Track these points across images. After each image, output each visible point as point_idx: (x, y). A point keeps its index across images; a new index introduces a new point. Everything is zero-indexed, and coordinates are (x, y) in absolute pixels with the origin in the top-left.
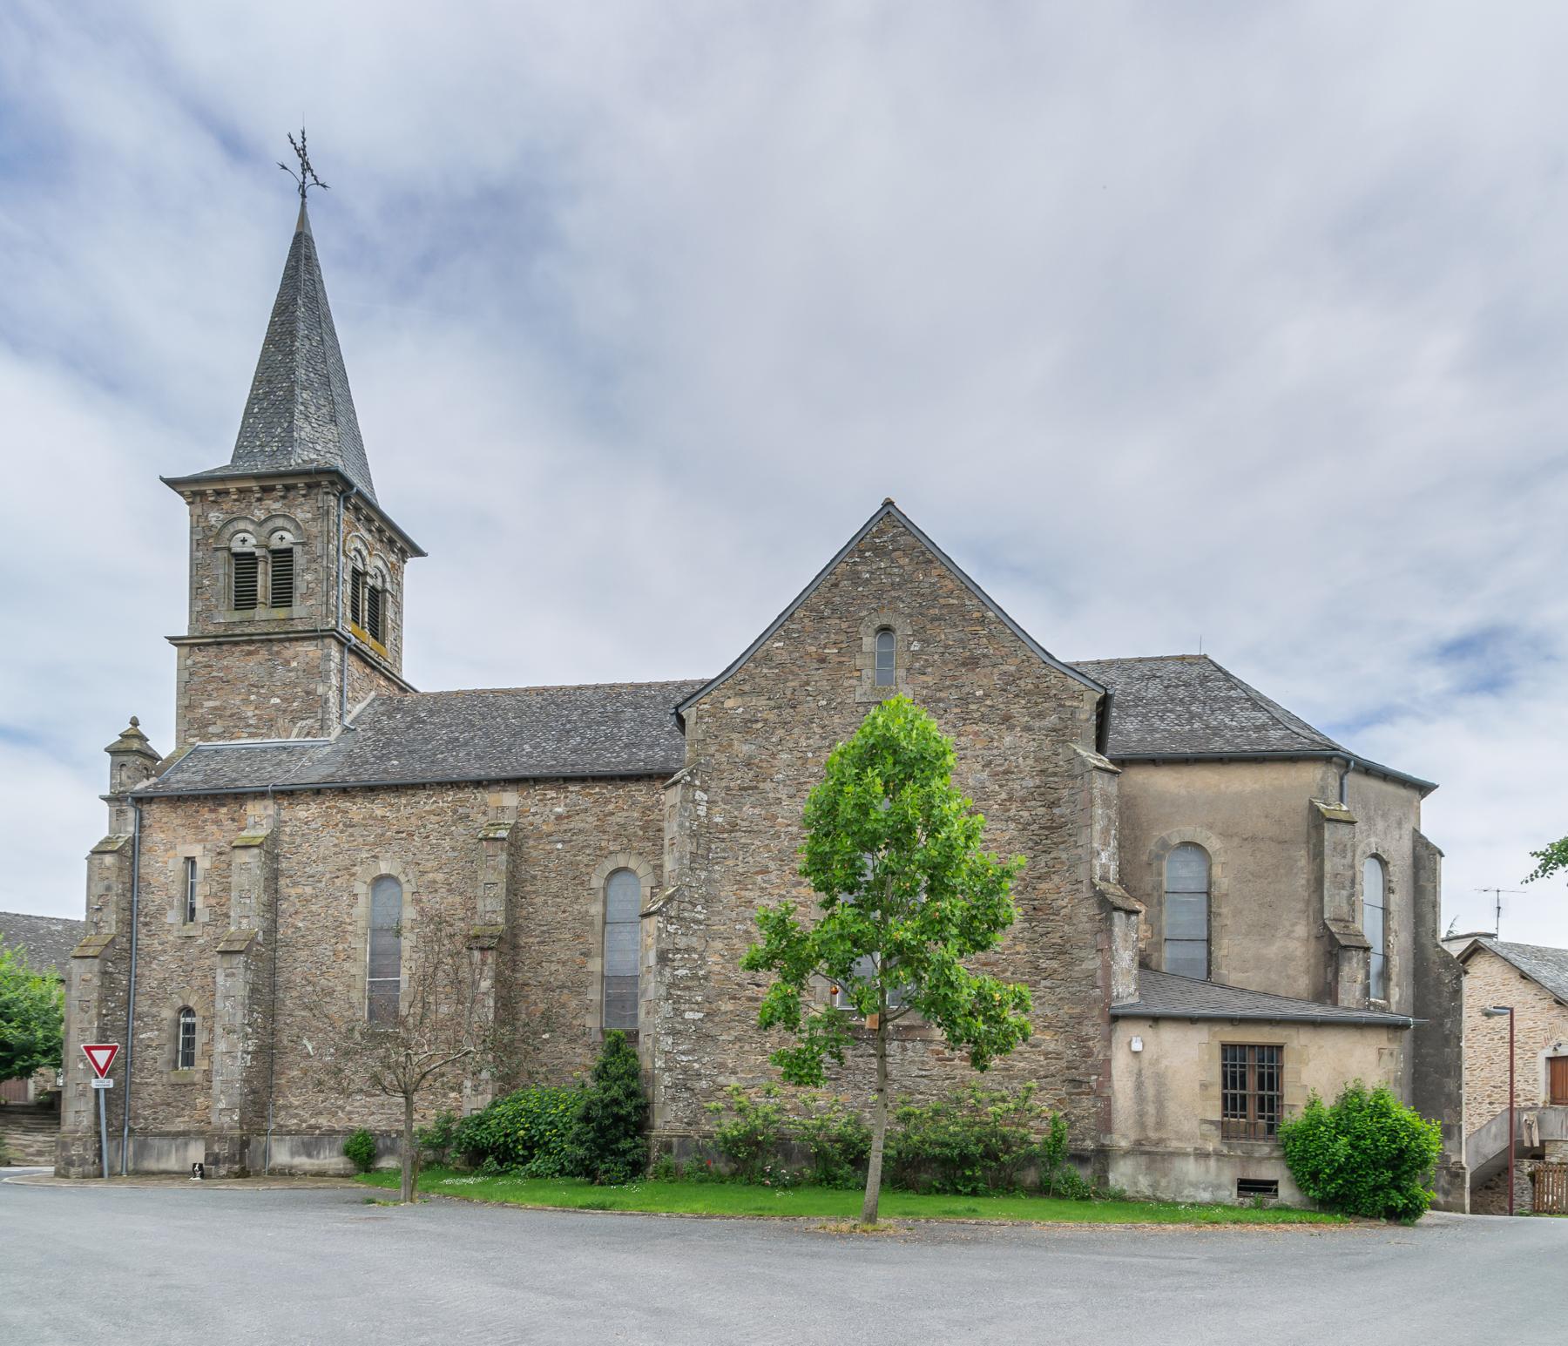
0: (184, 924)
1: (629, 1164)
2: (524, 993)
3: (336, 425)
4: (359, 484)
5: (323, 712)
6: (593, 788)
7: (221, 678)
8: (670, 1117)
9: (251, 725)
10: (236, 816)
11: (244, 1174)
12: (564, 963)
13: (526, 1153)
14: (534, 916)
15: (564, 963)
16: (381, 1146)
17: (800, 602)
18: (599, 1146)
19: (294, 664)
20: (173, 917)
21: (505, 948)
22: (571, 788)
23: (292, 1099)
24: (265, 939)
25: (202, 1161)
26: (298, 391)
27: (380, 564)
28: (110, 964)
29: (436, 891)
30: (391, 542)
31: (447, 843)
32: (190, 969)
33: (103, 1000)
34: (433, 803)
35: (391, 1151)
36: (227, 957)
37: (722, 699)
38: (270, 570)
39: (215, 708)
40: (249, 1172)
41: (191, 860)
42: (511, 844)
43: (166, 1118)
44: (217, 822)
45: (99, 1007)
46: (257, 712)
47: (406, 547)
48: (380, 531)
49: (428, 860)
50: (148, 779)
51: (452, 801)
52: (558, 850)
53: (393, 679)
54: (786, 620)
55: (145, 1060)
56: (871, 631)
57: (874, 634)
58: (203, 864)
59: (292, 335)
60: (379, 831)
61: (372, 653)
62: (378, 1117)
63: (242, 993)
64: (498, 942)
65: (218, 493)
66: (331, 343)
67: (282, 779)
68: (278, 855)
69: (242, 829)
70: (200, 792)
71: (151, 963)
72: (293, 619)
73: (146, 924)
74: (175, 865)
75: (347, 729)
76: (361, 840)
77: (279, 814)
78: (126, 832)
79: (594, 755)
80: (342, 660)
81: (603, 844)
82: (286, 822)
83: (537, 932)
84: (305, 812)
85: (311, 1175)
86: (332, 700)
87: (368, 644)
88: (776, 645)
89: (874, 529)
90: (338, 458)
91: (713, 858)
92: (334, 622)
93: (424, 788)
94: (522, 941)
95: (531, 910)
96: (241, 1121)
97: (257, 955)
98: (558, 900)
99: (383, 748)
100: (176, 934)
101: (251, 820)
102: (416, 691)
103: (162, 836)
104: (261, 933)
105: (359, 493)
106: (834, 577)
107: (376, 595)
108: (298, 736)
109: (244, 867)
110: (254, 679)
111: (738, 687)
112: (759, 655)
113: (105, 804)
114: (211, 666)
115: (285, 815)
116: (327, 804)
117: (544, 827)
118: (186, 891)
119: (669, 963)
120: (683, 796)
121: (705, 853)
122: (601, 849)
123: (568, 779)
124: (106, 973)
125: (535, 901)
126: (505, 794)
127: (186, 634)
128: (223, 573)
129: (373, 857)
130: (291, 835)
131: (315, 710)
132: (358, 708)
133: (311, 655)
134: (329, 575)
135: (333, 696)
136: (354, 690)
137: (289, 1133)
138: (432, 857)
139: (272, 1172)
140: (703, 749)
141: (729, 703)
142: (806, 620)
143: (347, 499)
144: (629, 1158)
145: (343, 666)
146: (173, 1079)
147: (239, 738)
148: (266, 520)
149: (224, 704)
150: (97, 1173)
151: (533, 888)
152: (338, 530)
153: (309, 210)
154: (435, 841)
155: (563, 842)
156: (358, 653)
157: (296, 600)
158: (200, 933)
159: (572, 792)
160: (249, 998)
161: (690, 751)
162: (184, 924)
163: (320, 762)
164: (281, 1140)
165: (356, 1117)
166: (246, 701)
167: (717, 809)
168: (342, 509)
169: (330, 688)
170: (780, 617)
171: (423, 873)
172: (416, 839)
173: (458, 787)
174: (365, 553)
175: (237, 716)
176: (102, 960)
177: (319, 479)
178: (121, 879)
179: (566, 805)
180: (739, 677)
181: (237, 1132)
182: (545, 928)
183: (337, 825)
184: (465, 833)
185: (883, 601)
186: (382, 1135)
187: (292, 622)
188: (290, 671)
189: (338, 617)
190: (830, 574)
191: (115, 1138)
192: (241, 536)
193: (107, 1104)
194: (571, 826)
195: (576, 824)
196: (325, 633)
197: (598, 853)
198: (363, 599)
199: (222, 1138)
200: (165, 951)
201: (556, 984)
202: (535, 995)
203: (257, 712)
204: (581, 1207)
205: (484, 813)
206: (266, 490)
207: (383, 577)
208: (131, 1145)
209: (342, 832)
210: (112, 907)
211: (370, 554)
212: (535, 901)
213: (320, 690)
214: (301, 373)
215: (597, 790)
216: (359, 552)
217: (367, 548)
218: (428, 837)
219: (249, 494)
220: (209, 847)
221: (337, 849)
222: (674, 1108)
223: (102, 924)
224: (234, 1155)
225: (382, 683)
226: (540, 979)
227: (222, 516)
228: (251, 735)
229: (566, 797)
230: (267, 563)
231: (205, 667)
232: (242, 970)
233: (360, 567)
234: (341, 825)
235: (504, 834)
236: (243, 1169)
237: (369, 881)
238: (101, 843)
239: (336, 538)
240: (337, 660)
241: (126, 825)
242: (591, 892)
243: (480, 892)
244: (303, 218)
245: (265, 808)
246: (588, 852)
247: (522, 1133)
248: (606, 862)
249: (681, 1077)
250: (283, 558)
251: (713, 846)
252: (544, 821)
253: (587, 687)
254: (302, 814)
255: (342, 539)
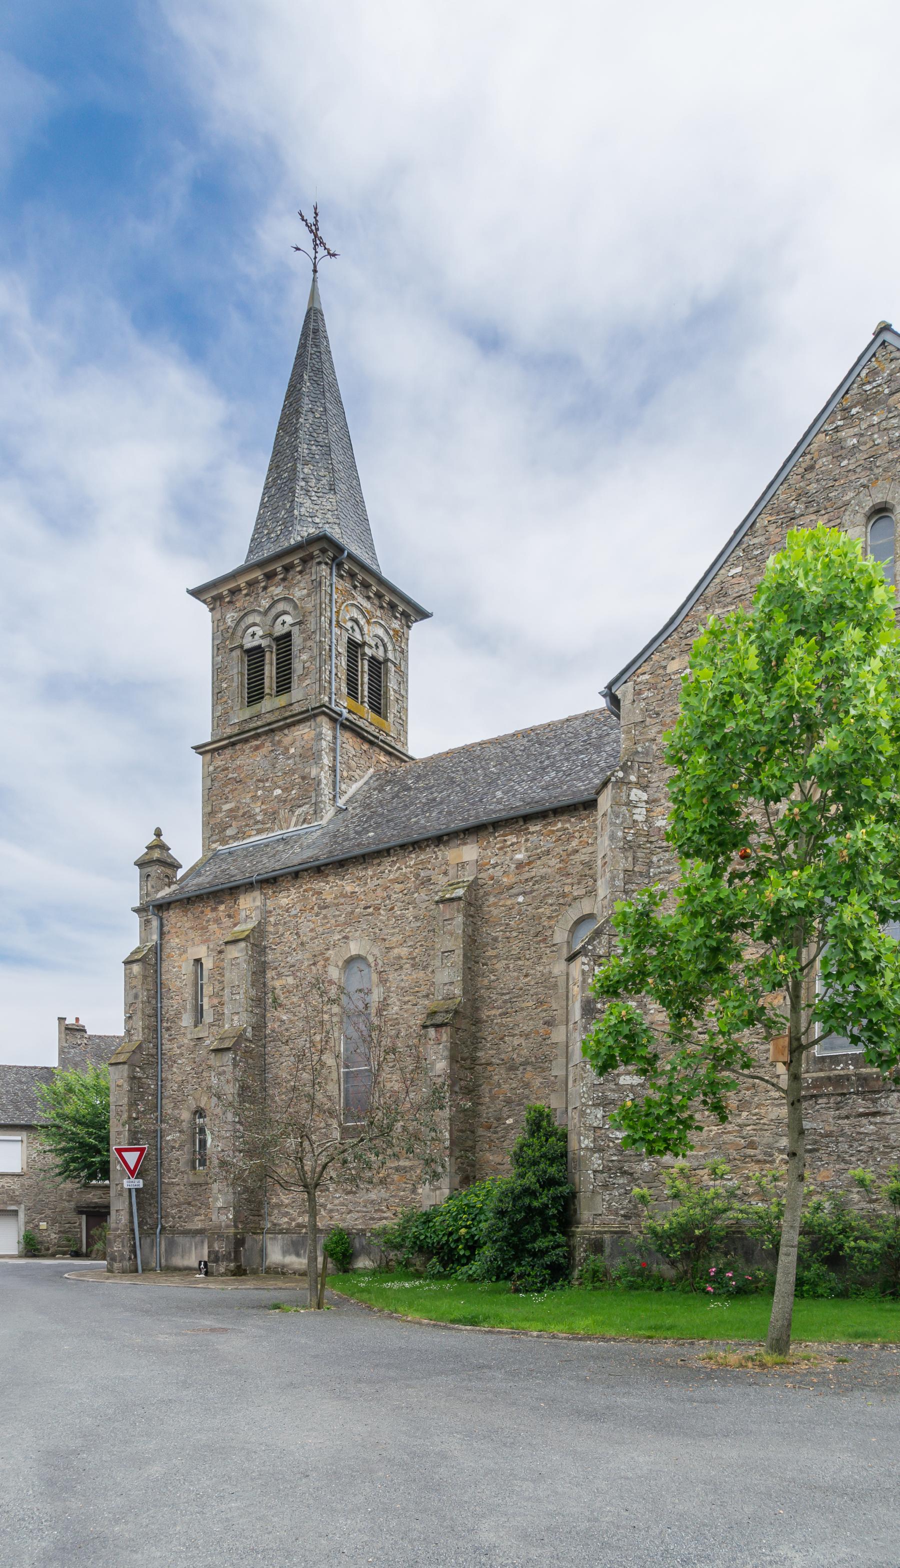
0: (196, 1026)
1: (548, 1267)
2: (487, 1074)
3: (335, 493)
4: (354, 548)
5: (316, 795)
6: (555, 825)
7: (235, 779)
8: (601, 1208)
9: (259, 821)
10: (232, 911)
11: (239, 1272)
12: (527, 1036)
13: (468, 1253)
14: (496, 984)
15: (527, 1036)
16: (358, 1246)
17: (763, 503)
18: (515, 1247)
19: (292, 751)
20: (187, 1020)
21: (464, 1024)
22: (532, 829)
23: (283, 1197)
24: (254, 1035)
25: (206, 1259)
26: (299, 467)
27: (380, 632)
28: (138, 1069)
29: (401, 967)
30: (393, 606)
31: (410, 913)
32: (200, 1070)
33: (132, 1104)
34: (396, 871)
35: (366, 1251)
36: (219, 1055)
37: (664, 663)
38: (274, 658)
39: (231, 810)
40: (245, 1270)
41: (198, 961)
42: (470, 904)
43: (187, 1217)
44: (217, 921)
45: (129, 1111)
46: (263, 807)
47: (409, 611)
48: (379, 596)
49: (393, 934)
50: (169, 887)
51: (415, 864)
52: (519, 903)
53: (396, 755)
54: (746, 534)
55: (171, 1161)
56: (860, 518)
57: (864, 520)
58: (208, 964)
59: (298, 413)
60: (349, 909)
61: (371, 729)
62: (355, 1215)
63: (232, 1091)
64: (454, 1017)
65: (233, 592)
66: (335, 411)
67: (268, 865)
68: (265, 947)
69: (235, 925)
70: (202, 892)
71: (172, 1066)
72: (291, 705)
73: (168, 1029)
74: (187, 968)
75: (340, 810)
76: (333, 921)
77: (265, 905)
78: (152, 940)
79: (565, 787)
80: (335, 738)
81: (567, 889)
82: (271, 912)
83: (499, 1003)
84: (287, 898)
85: (300, 1275)
86: (324, 781)
87: (367, 718)
88: (733, 572)
89: (863, 374)
90: (336, 527)
91: (655, 875)
92: (326, 699)
93: (389, 855)
94: (485, 1014)
95: (493, 978)
96: (236, 1220)
97: (246, 1052)
98: (520, 963)
99: (366, 822)
100: (189, 1037)
101: (243, 914)
102: (412, 759)
103: (177, 940)
104: (250, 1029)
105: (351, 557)
106: (809, 457)
107: (377, 666)
108: (295, 825)
109: (234, 963)
110: (260, 773)
111: (684, 642)
112: (711, 591)
113: (136, 915)
114: (227, 769)
115: (270, 905)
116: (304, 887)
117: (505, 880)
118: (197, 993)
119: (598, 1015)
120: (614, 798)
121: (644, 869)
122: (564, 895)
123: (527, 818)
124: (134, 1078)
125: (496, 967)
126: (465, 847)
127: (209, 740)
128: (237, 669)
129: (344, 938)
130: (276, 925)
131: (309, 795)
132: (355, 787)
133: (306, 737)
134: (321, 649)
135: (325, 778)
136: (349, 768)
137: (281, 1232)
138: (397, 930)
139: (268, 1271)
140: (641, 733)
141: (673, 666)
142: (771, 528)
143: (340, 566)
144: (547, 1260)
145: (335, 743)
146: (192, 1179)
147: (250, 836)
148: (270, 608)
149: (238, 805)
150: (133, 1268)
151: (494, 953)
152: (331, 600)
153: (319, 284)
154: (399, 913)
155: (524, 893)
156: (350, 727)
157: (294, 684)
158: (206, 1034)
159: (533, 833)
160: (239, 1095)
161: (625, 740)
162: (196, 1026)
163: (308, 847)
164: (275, 1239)
165: (336, 1215)
166: (255, 798)
167: (659, 809)
168: (335, 579)
169: (322, 768)
170: (736, 532)
171: (389, 949)
172: (382, 912)
173: (420, 848)
174: (362, 622)
175: (248, 815)
176: (129, 1065)
177: (311, 550)
178: (145, 987)
179: (527, 850)
180: (686, 628)
181: (232, 1230)
182: (507, 997)
183: (312, 908)
184: (427, 898)
185: (876, 471)
186: (357, 1234)
187: (291, 708)
188: (289, 758)
189: (331, 693)
190: (804, 454)
191: (149, 1235)
192: (250, 630)
193: (138, 1203)
194: (533, 874)
195: (538, 870)
196: (315, 712)
197: (561, 901)
198: (362, 672)
199: (220, 1236)
200: (182, 1054)
201: (519, 1060)
202: (498, 1074)
203: (263, 807)
204: (453, 1321)
205: (445, 873)
206: (270, 576)
207: (385, 646)
208: (163, 1242)
209: (317, 915)
210: (139, 1014)
211: (368, 622)
212: (496, 967)
213: (314, 773)
214: (303, 449)
215: (559, 825)
216: (356, 621)
217: (365, 616)
218: (392, 909)
219: (256, 585)
220: (211, 946)
221: (313, 934)
222: (607, 1198)
223: (132, 1032)
224: (230, 1253)
225: (382, 758)
226: (503, 1056)
227: (236, 615)
228: (259, 832)
229: (527, 840)
230: (272, 652)
231: (223, 770)
232: (231, 1067)
233: (358, 637)
234: (316, 908)
235: (460, 892)
236: (239, 1267)
237: (340, 964)
238: (132, 953)
239: (328, 609)
240: (330, 738)
241: (151, 934)
242: (554, 949)
243: (437, 963)
244: (314, 294)
245: (254, 900)
246: (550, 901)
247: (463, 1231)
248: (570, 910)
249: (615, 1158)
250: (284, 641)
251: (655, 859)
252: (505, 872)
253: (576, 718)
254: (284, 901)
255: (334, 610)
